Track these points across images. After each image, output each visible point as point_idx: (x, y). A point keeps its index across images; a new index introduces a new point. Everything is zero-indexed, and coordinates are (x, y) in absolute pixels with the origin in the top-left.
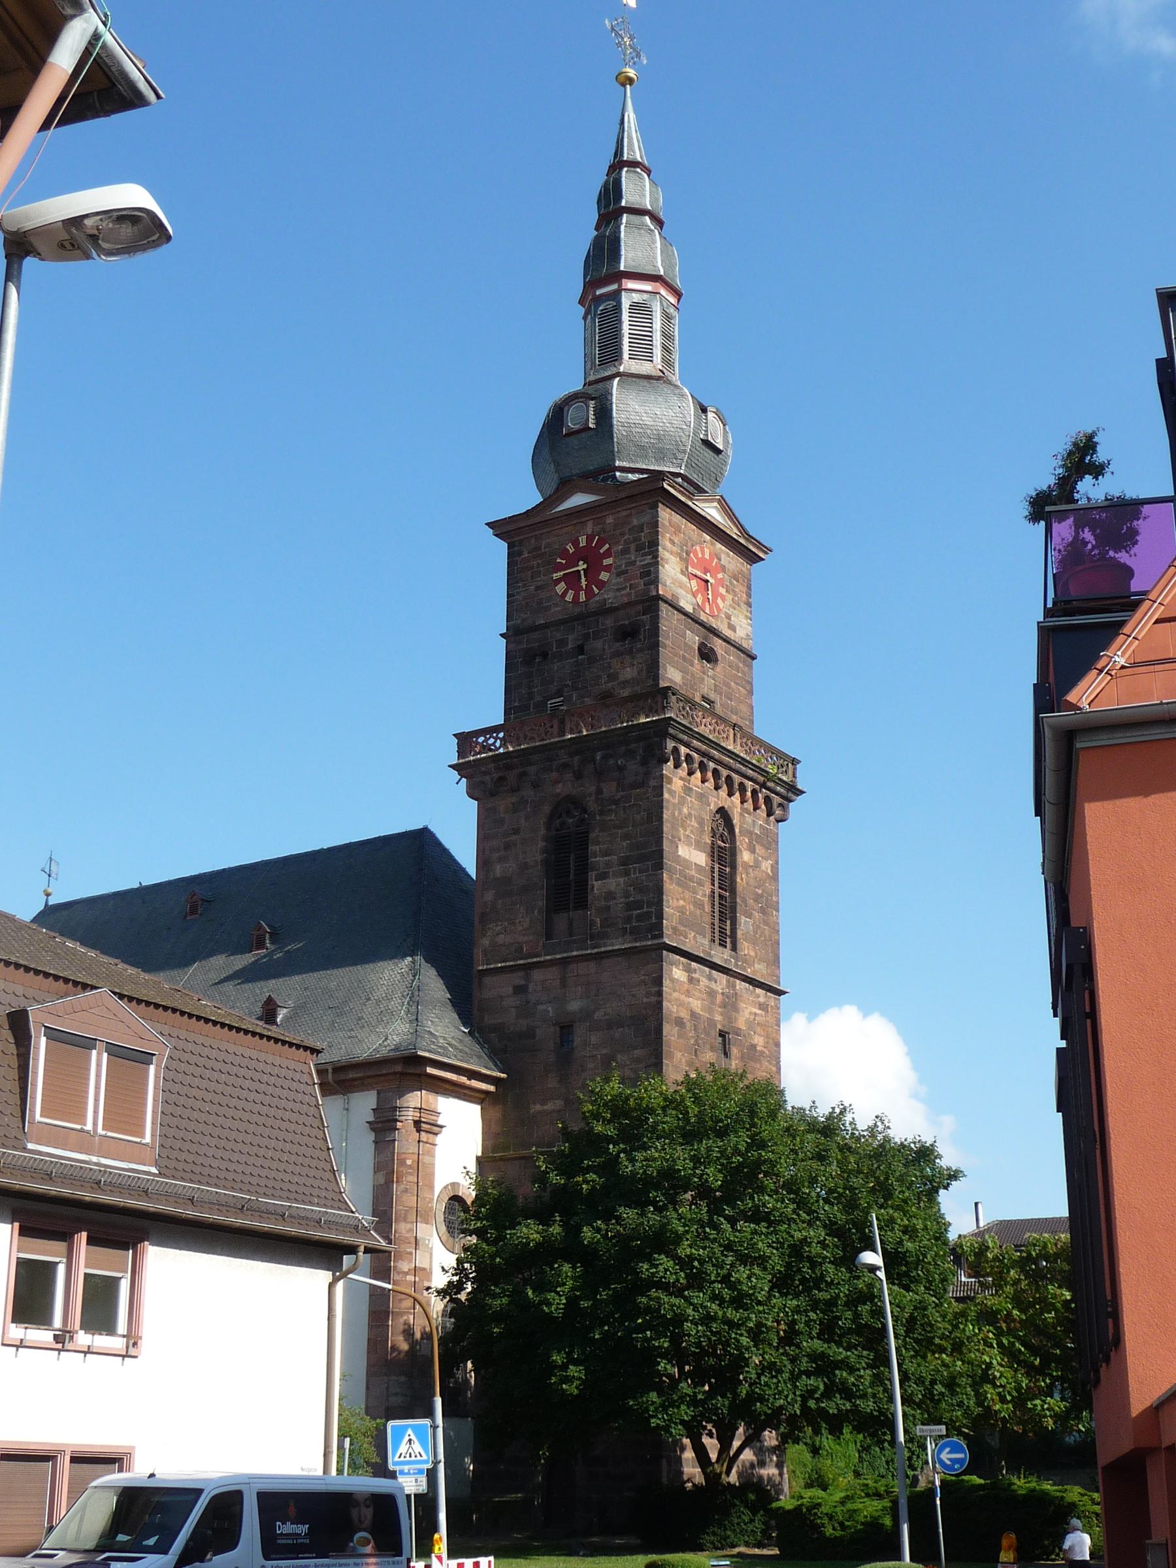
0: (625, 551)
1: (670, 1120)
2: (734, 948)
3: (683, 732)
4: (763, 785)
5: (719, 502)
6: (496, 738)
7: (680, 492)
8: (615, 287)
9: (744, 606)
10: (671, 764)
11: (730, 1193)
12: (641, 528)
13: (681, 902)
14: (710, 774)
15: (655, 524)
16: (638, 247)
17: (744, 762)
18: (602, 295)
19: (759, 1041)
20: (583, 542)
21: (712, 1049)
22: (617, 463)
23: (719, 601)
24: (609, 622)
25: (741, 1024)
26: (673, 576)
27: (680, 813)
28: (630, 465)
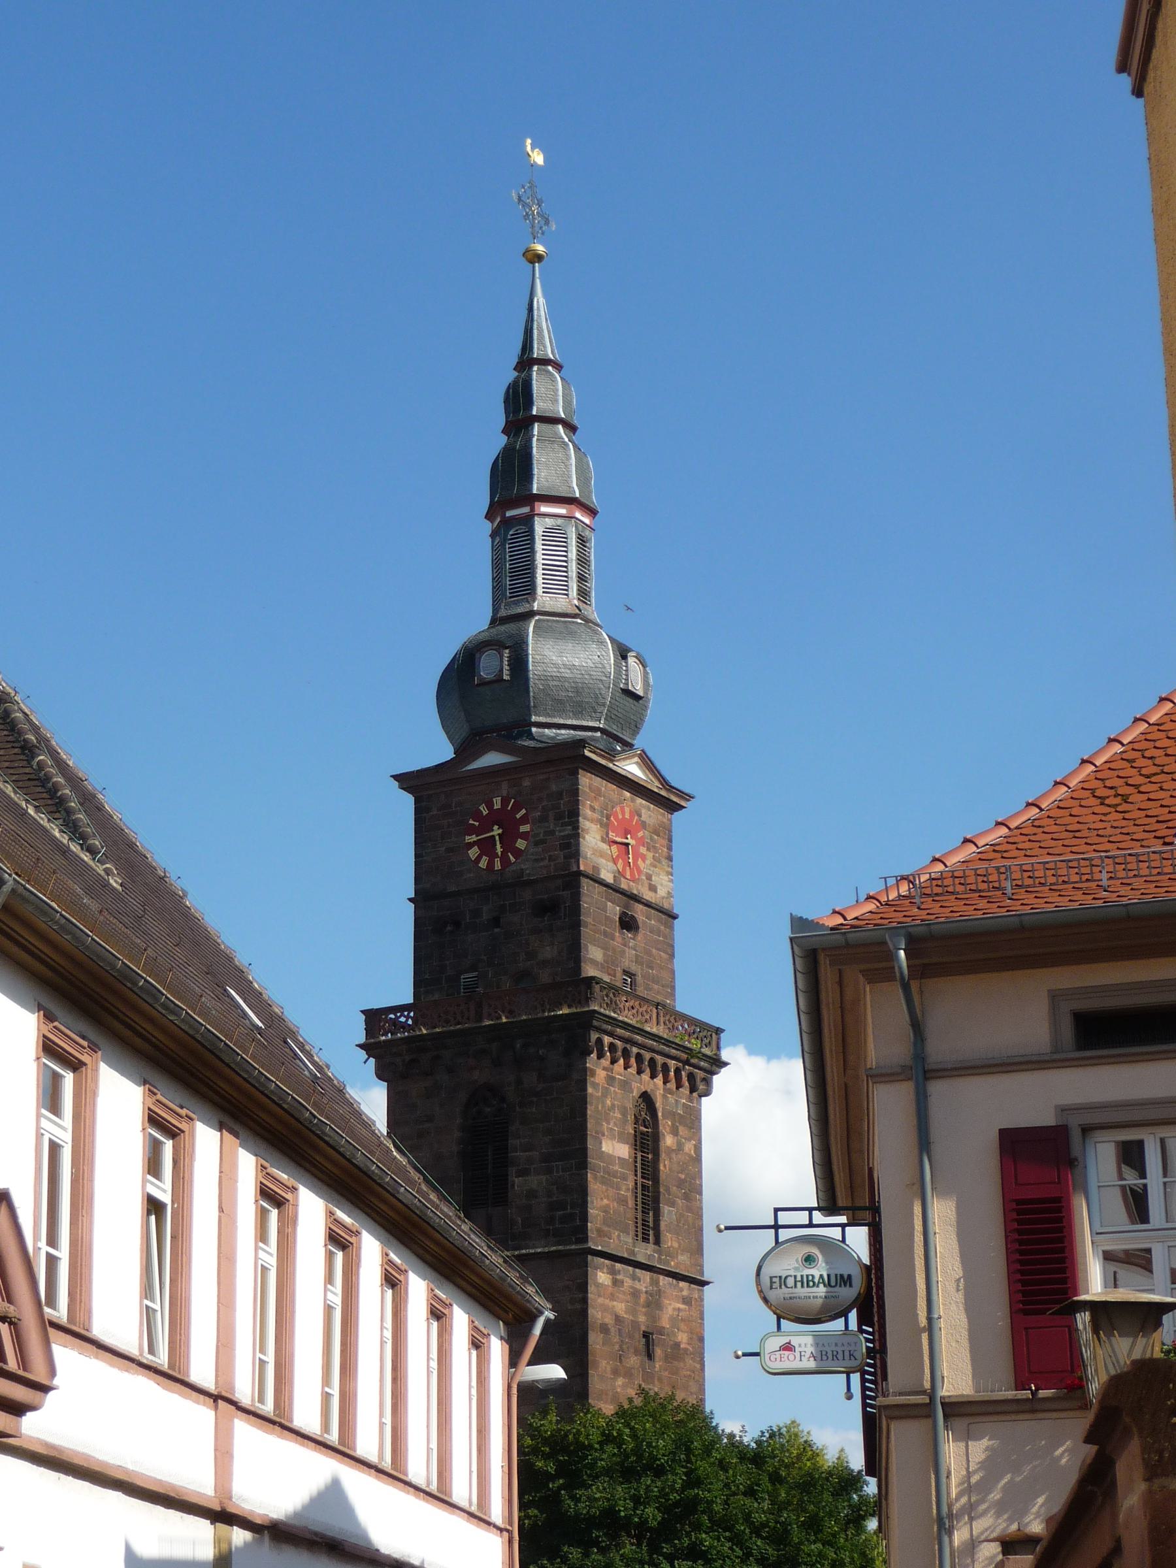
0: (543, 819)
1: (606, 1457)
2: (657, 1242)
3: (607, 1023)
4: (687, 1062)
5: (640, 756)
6: (408, 1017)
7: (601, 756)
8: (525, 510)
9: (664, 862)
10: (594, 1056)
11: (666, 1531)
12: (560, 795)
13: (605, 1201)
14: (633, 1061)
15: (575, 792)
16: (552, 466)
17: (668, 1043)
18: (513, 517)
19: (682, 1338)
20: (497, 803)
21: (636, 1352)
22: (534, 719)
23: (640, 862)
25: (665, 1323)
26: (595, 846)
27: (604, 1103)
28: (550, 729)
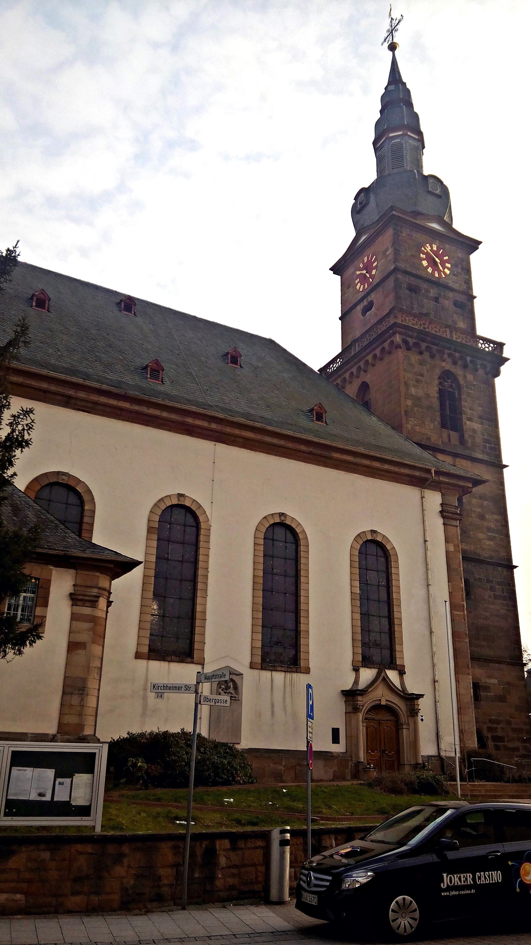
24: (359, 308)
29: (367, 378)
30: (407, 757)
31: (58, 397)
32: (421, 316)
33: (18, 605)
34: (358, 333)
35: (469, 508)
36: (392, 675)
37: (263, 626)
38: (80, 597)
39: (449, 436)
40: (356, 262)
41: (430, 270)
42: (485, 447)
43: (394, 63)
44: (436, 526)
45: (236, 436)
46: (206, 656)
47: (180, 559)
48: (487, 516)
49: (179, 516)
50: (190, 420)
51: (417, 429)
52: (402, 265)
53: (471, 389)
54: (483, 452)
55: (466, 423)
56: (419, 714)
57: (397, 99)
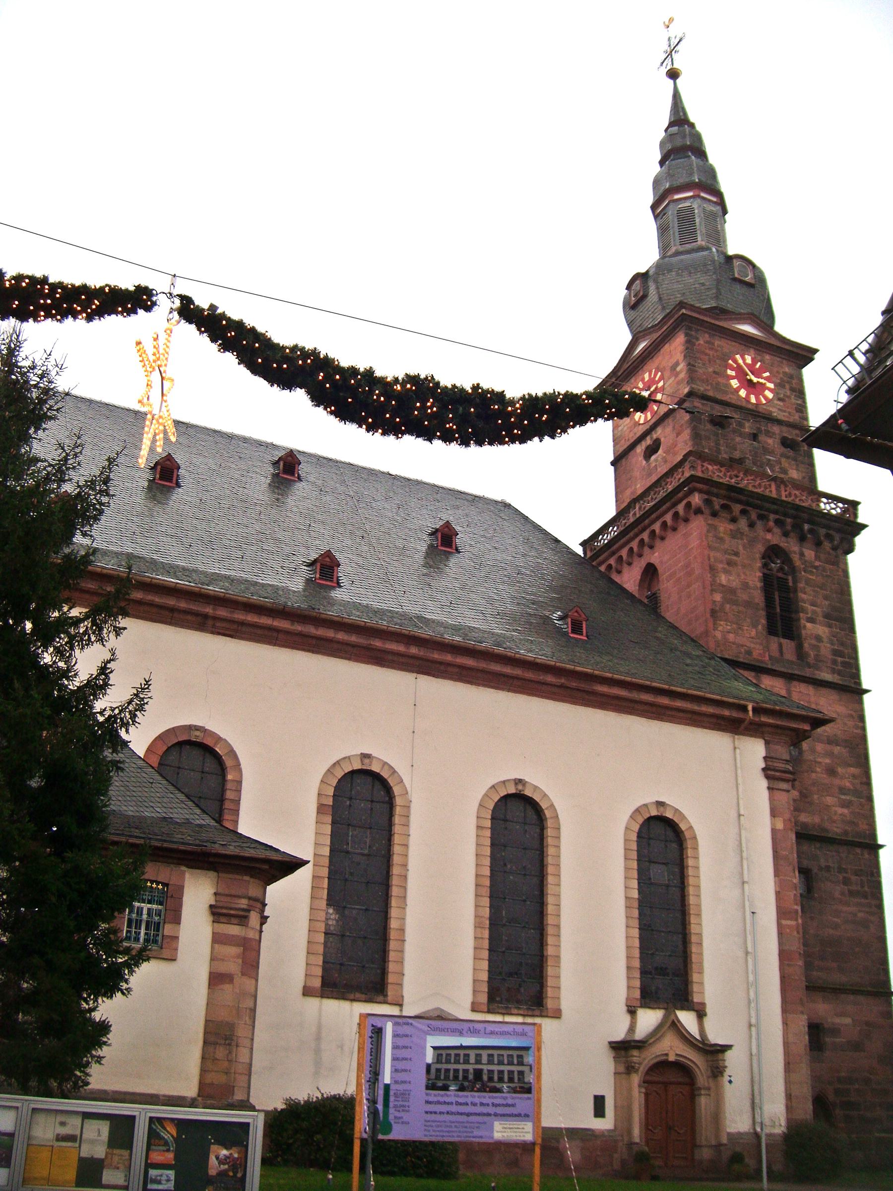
24: (640, 449)
29: (655, 557)
30: (705, 1134)
31: (189, 617)
32: (734, 463)
33: (141, 921)
34: (639, 488)
35: (811, 758)
36: (687, 1019)
37: (490, 950)
38: (224, 911)
39: (780, 646)
40: (632, 380)
41: (743, 393)
42: (834, 662)
43: (676, 96)
44: (758, 790)
45: (449, 664)
46: (405, 994)
47: (366, 852)
48: (839, 770)
49: (362, 786)
50: (378, 643)
51: (731, 637)
52: (701, 388)
53: (811, 573)
54: (833, 671)
55: (805, 627)
56: (726, 1074)
57: (683, 145)
